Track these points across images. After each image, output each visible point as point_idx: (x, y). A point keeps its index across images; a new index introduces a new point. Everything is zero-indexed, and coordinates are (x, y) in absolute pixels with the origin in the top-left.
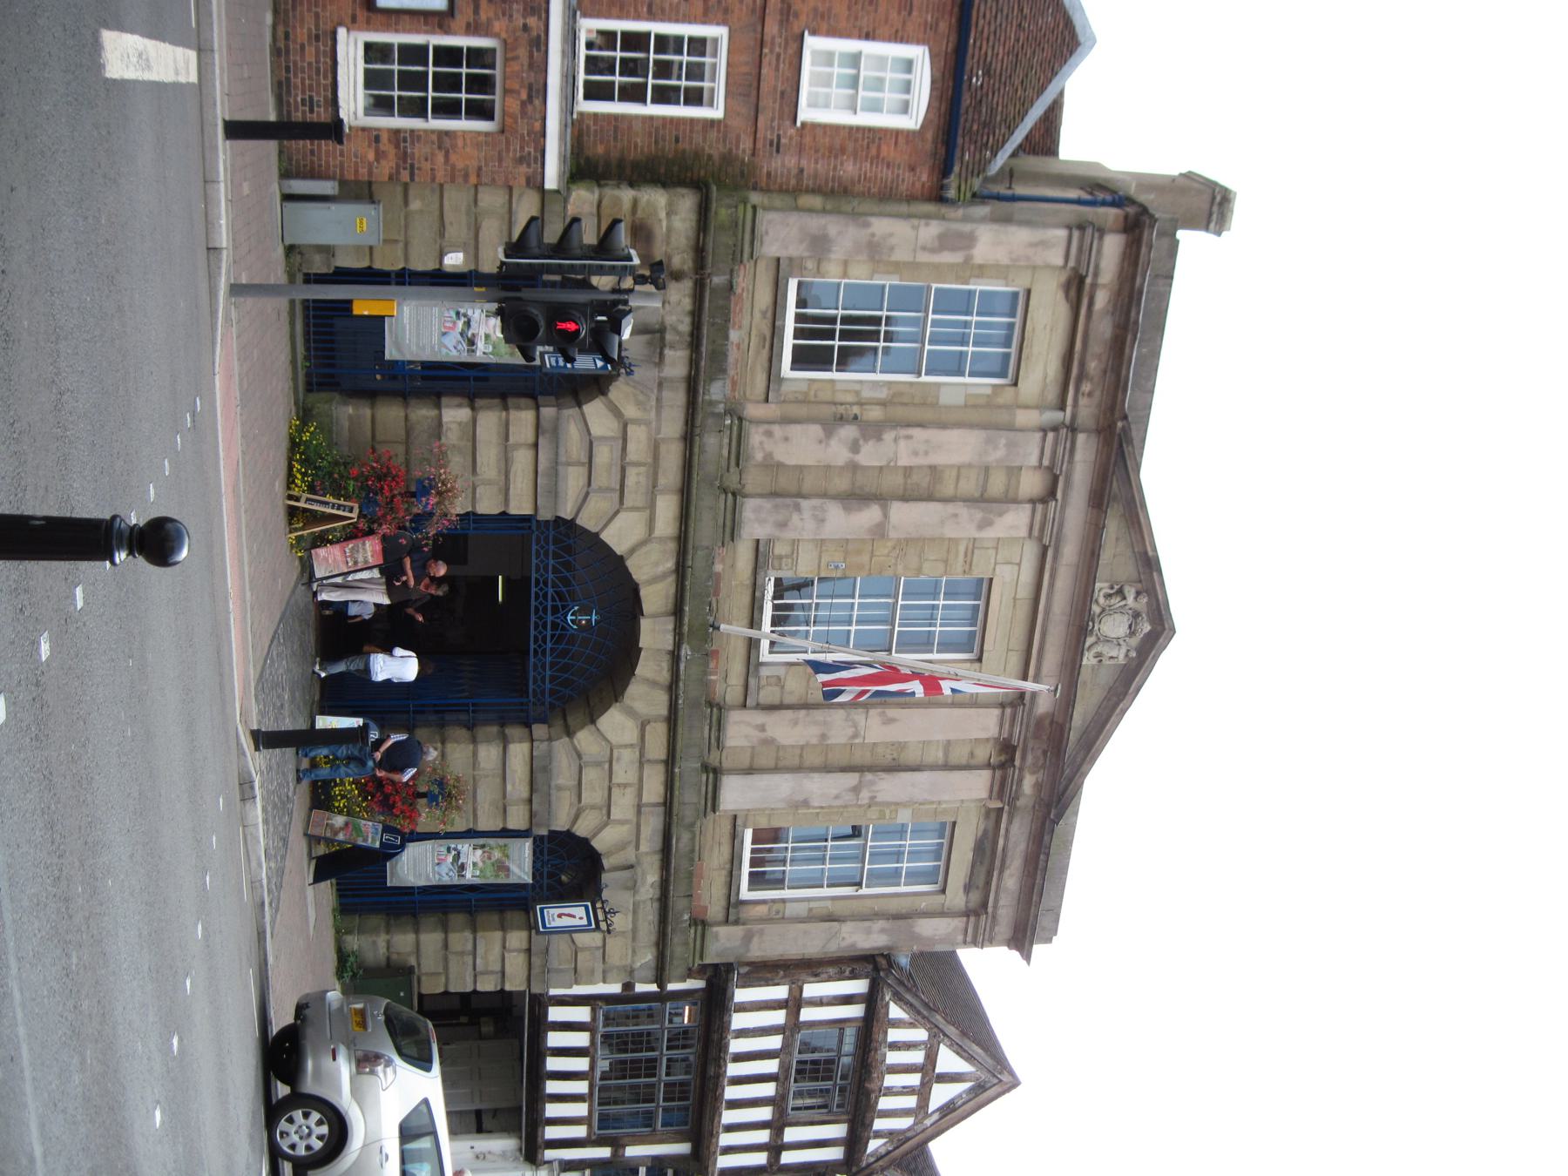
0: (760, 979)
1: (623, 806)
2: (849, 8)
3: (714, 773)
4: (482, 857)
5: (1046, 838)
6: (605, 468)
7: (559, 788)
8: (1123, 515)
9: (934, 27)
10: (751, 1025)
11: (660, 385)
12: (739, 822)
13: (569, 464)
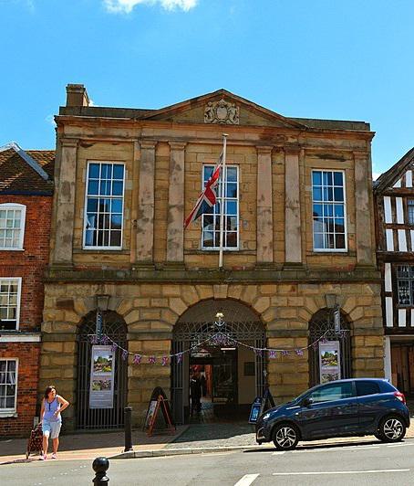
6: (154, 311)
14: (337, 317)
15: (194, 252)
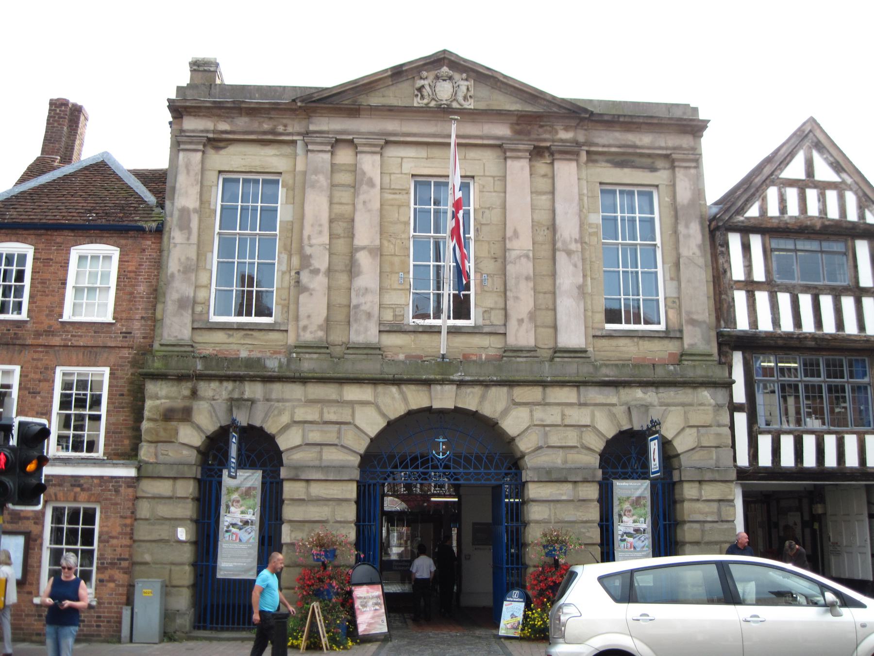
0: (728, 311)
2: (47, 295)
3: (558, 352)
4: (629, 516)
5: (606, 118)
6: (328, 435)
7: (565, 462)
8: (367, 94)
9: (59, 245)
11: (268, 400)
12: (599, 333)
13: (321, 459)
14: (654, 446)
15: (397, 329)
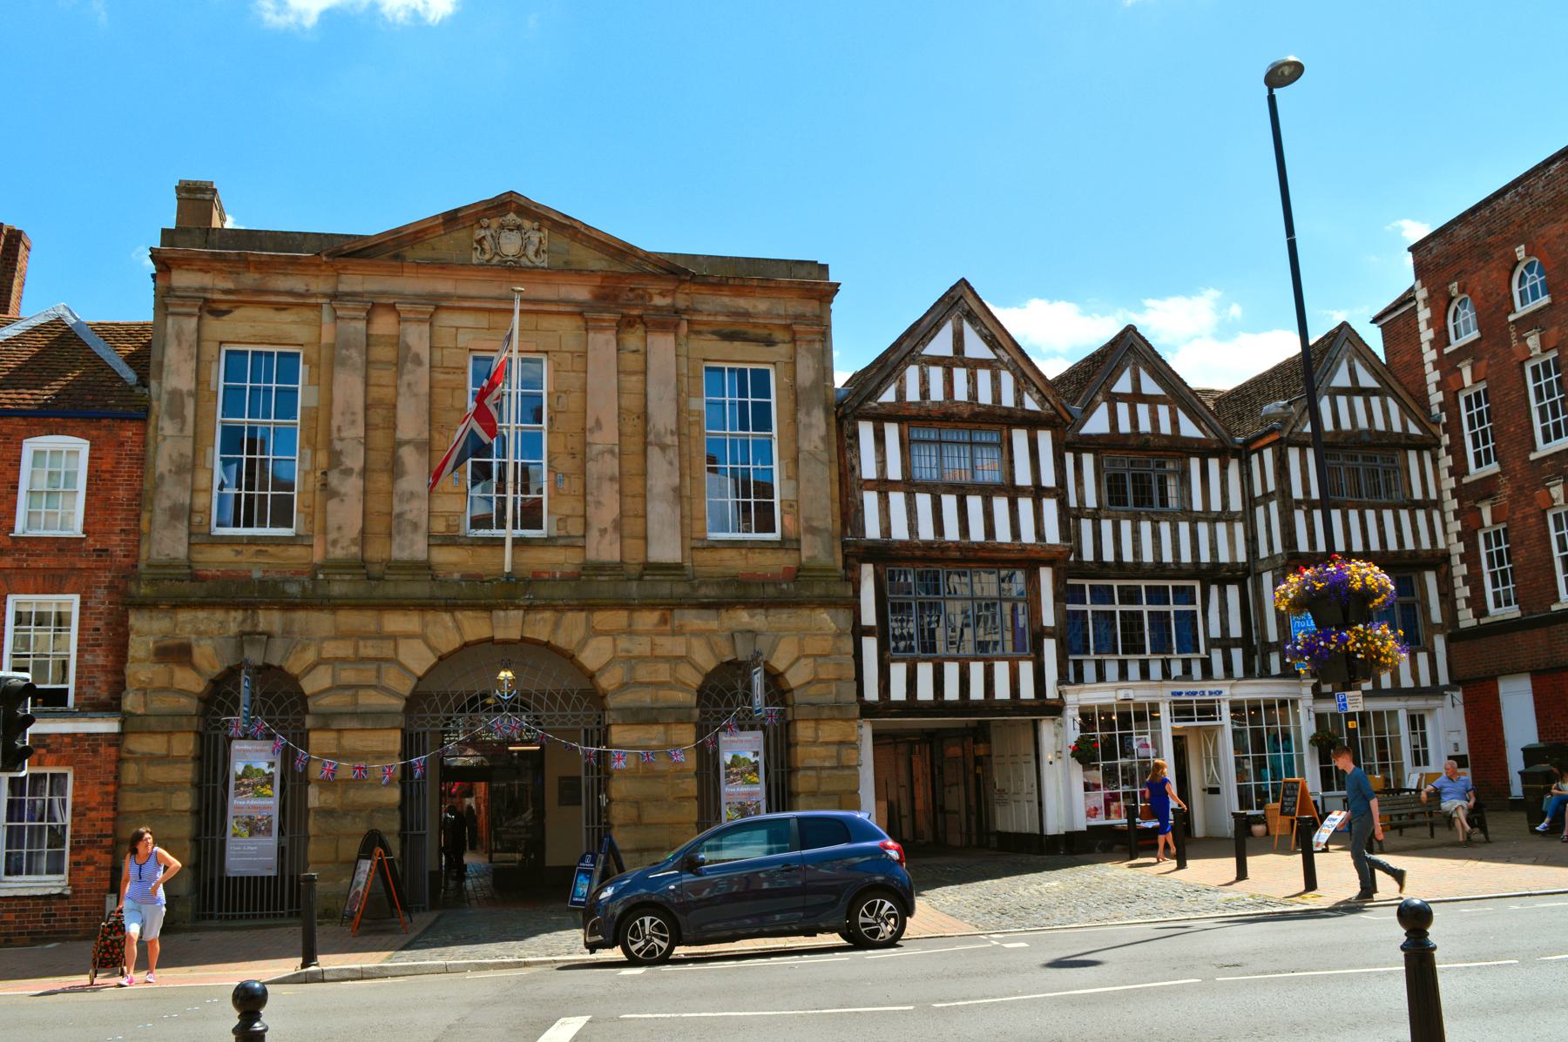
1: (671, 645)
10: (905, 522)
